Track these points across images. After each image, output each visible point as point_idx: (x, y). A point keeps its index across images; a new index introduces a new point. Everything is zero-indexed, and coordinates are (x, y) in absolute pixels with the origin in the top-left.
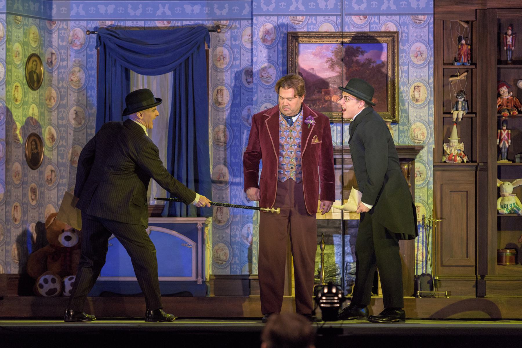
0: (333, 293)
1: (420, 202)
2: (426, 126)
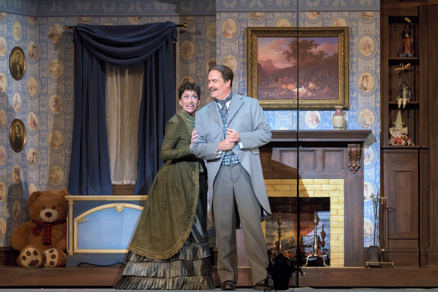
1: (368, 181)
2: (373, 112)
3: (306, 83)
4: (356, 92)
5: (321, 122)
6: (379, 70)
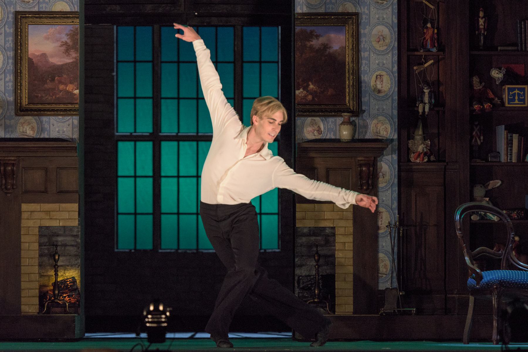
0: (160, 311)
1: (383, 207)
2: (389, 121)
3: (305, 84)
4: (367, 95)
5: (324, 133)
6: (396, 69)
